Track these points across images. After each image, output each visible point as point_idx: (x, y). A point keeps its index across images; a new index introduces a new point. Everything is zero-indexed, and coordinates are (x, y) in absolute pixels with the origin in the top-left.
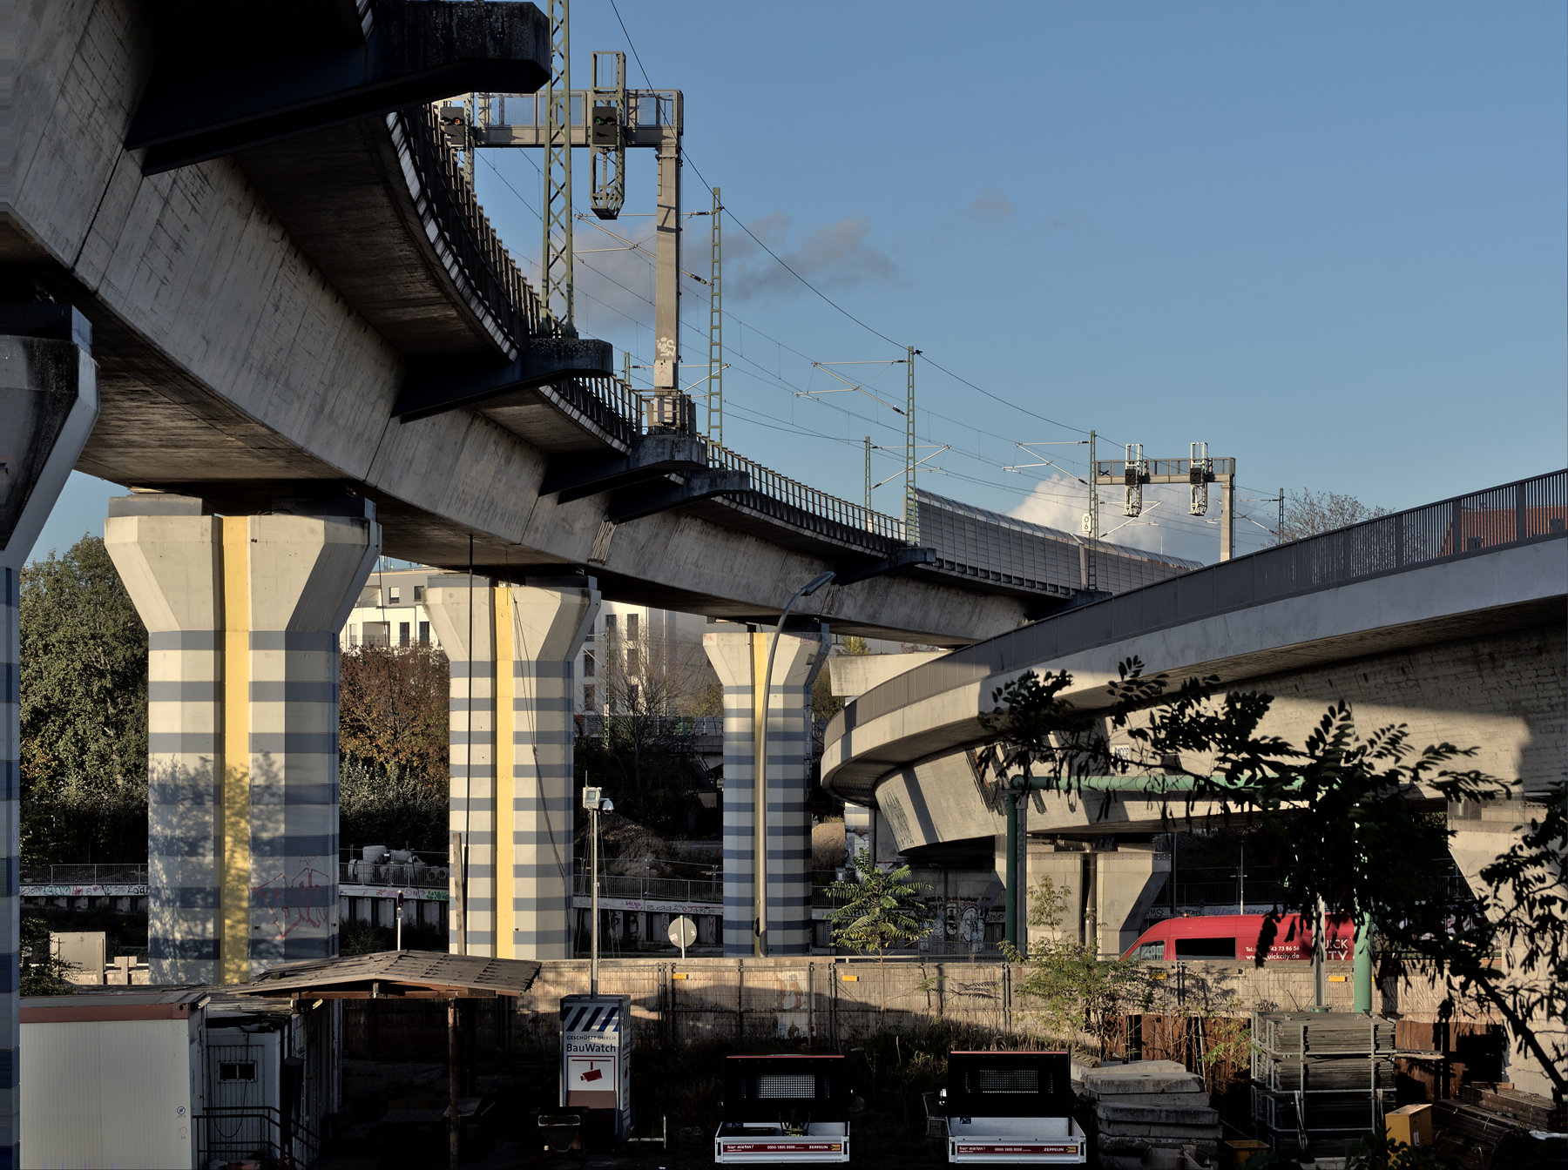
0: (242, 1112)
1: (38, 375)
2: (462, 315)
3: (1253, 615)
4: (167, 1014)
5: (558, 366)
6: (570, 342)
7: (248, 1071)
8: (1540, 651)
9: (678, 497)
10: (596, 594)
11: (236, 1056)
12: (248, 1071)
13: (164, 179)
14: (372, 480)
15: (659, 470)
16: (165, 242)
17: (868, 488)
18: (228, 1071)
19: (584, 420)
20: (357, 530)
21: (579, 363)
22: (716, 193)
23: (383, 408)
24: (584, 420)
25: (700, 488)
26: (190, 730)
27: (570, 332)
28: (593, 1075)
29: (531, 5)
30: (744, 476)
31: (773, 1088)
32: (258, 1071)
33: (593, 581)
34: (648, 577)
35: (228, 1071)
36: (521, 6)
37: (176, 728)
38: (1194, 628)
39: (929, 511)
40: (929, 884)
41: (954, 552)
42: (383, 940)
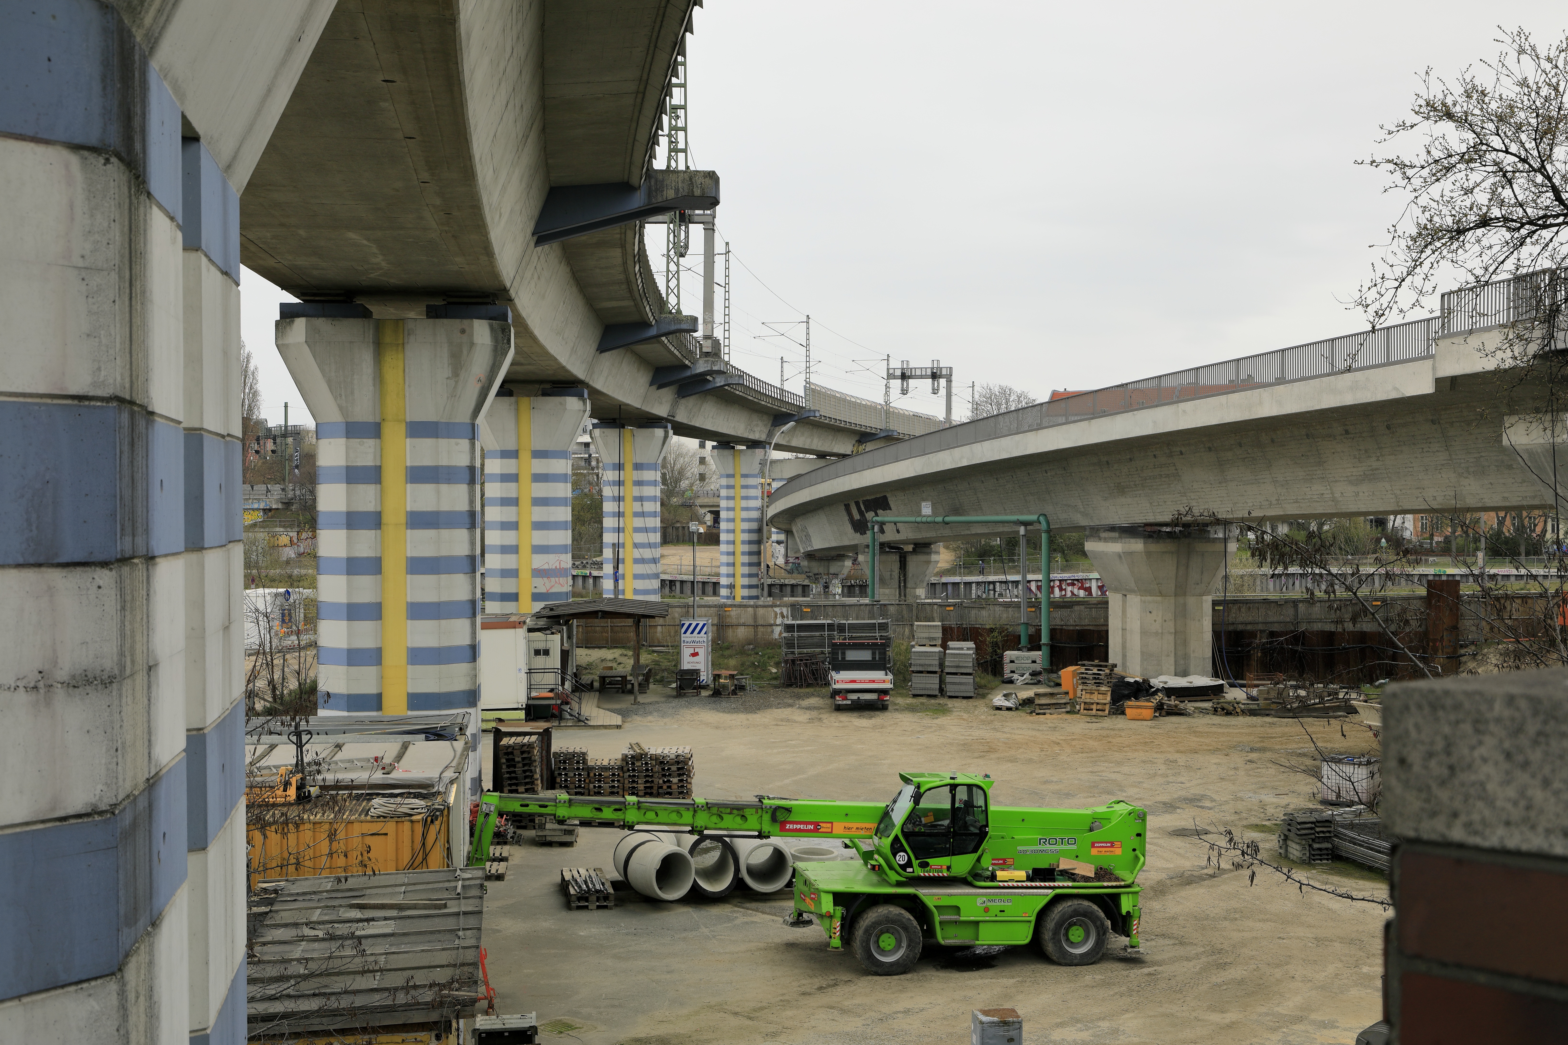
0: (544, 671)
1: (495, 339)
2: (636, 305)
3: (996, 443)
4: (514, 626)
5: (673, 327)
6: (678, 316)
7: (546, 652)
8: (1131, 460)
9: (710, 386)
10: (671, 432)
11: (541, 646)
12: (546, 652)
13: (539, 249)
14: (587, 380)
15: (703, 374)
16: (536, 276)
17: (782, 380)
18: (537, 652)
19: (676, 352)
20: (581, 403)
21: (684, 326)
22: (727, 244)
23: (595, 346)
24: (676, 352)
25: (720, 381)
26: (504, 496)
27: (679, 311)
28: (695, 654)
29: (714, 172)
30: (741, 377)
31: (852, 655)
32: (551, 652)
33: (669, 426)
34: (692, 424)
35: (537, 652)
36: (709, 172)
37: (498, 495)
38: (966, 448)
39: (811, 390)
40: (816, 567)
41: (826, 411)
42: (1013, 582)
